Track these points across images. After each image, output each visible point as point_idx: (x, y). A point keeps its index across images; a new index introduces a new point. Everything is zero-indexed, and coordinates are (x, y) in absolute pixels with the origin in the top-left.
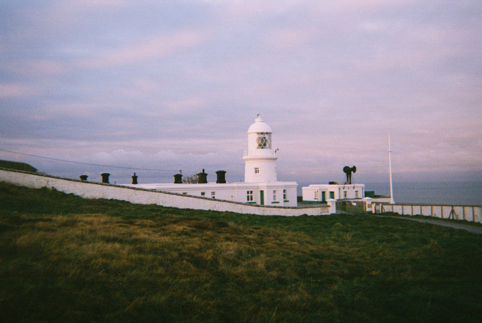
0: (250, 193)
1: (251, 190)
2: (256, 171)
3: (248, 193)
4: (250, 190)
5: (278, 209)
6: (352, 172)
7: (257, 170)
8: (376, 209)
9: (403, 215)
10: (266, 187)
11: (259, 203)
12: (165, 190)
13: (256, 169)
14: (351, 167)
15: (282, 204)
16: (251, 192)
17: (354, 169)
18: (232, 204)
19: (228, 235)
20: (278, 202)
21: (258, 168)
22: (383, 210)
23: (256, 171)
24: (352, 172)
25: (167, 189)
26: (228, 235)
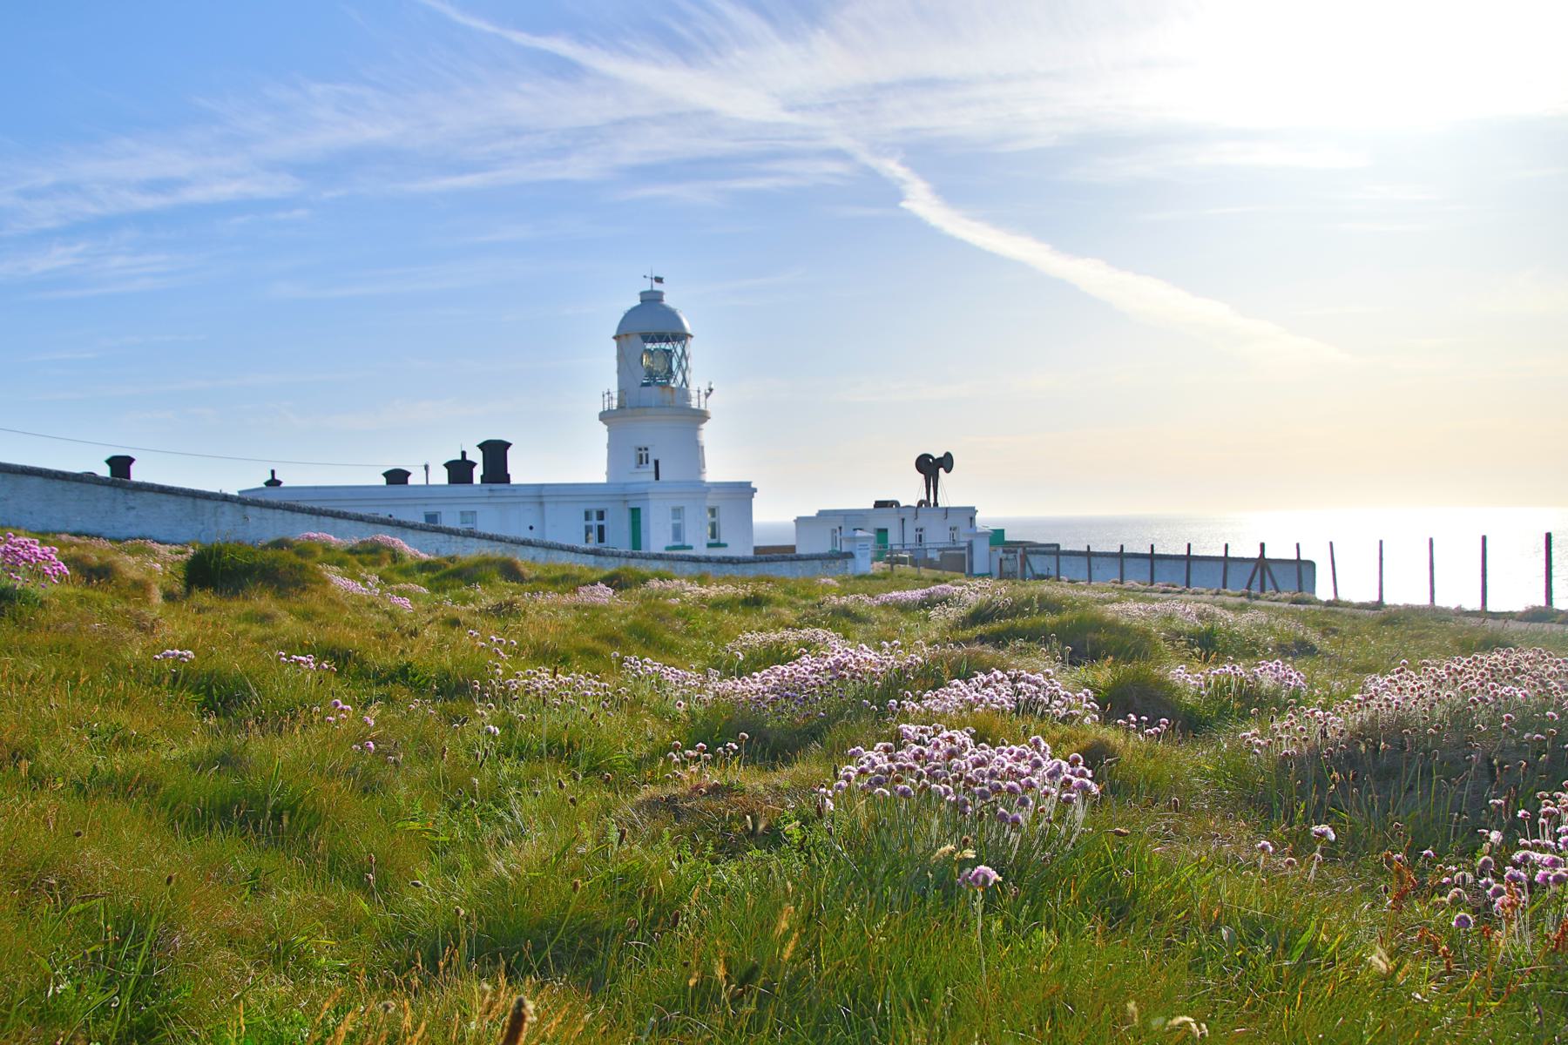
0: (594, 516)
1: (601, 507)
2: (641, 456)
3: (587, 516)
4: (595, 507)
5: (667, 563)
6: (941, 471)
7: (644, 453)
8: (1004, 569)
9: (1483, 613)
10: (650, 497)
11: (625, 547)
12: (255, 494)
13: (640, 449)
14: (938, 454)
15: (701, 550)
16: (601, 515)
17: (947, 462)
18: (499, 543)
19: (923, 727)
20: (690, 548)
21: (646, 449)
22: (1028, 568)
23: (641, 456)
24: (941, 471)
25: (515, 503)
26: (923, 727)
